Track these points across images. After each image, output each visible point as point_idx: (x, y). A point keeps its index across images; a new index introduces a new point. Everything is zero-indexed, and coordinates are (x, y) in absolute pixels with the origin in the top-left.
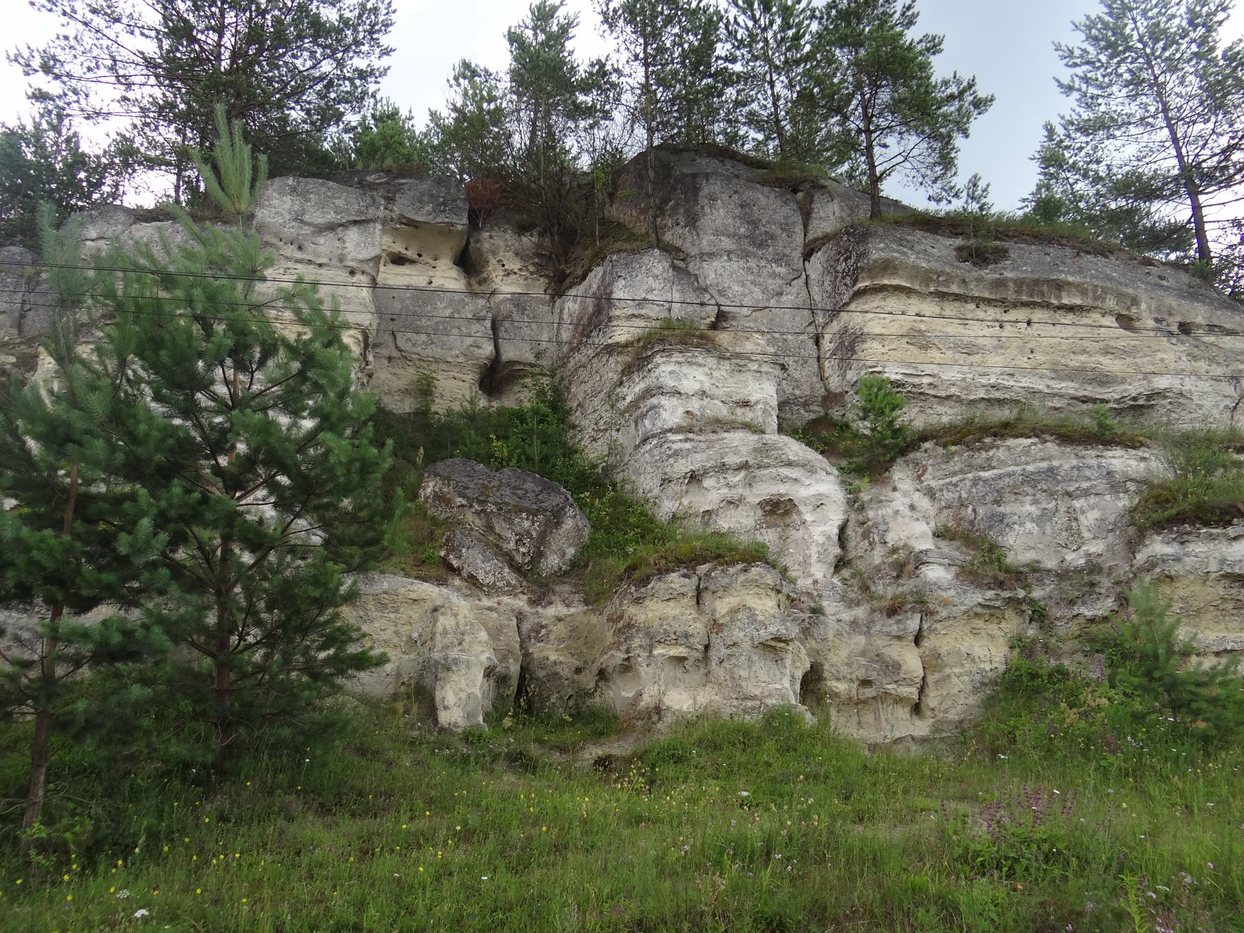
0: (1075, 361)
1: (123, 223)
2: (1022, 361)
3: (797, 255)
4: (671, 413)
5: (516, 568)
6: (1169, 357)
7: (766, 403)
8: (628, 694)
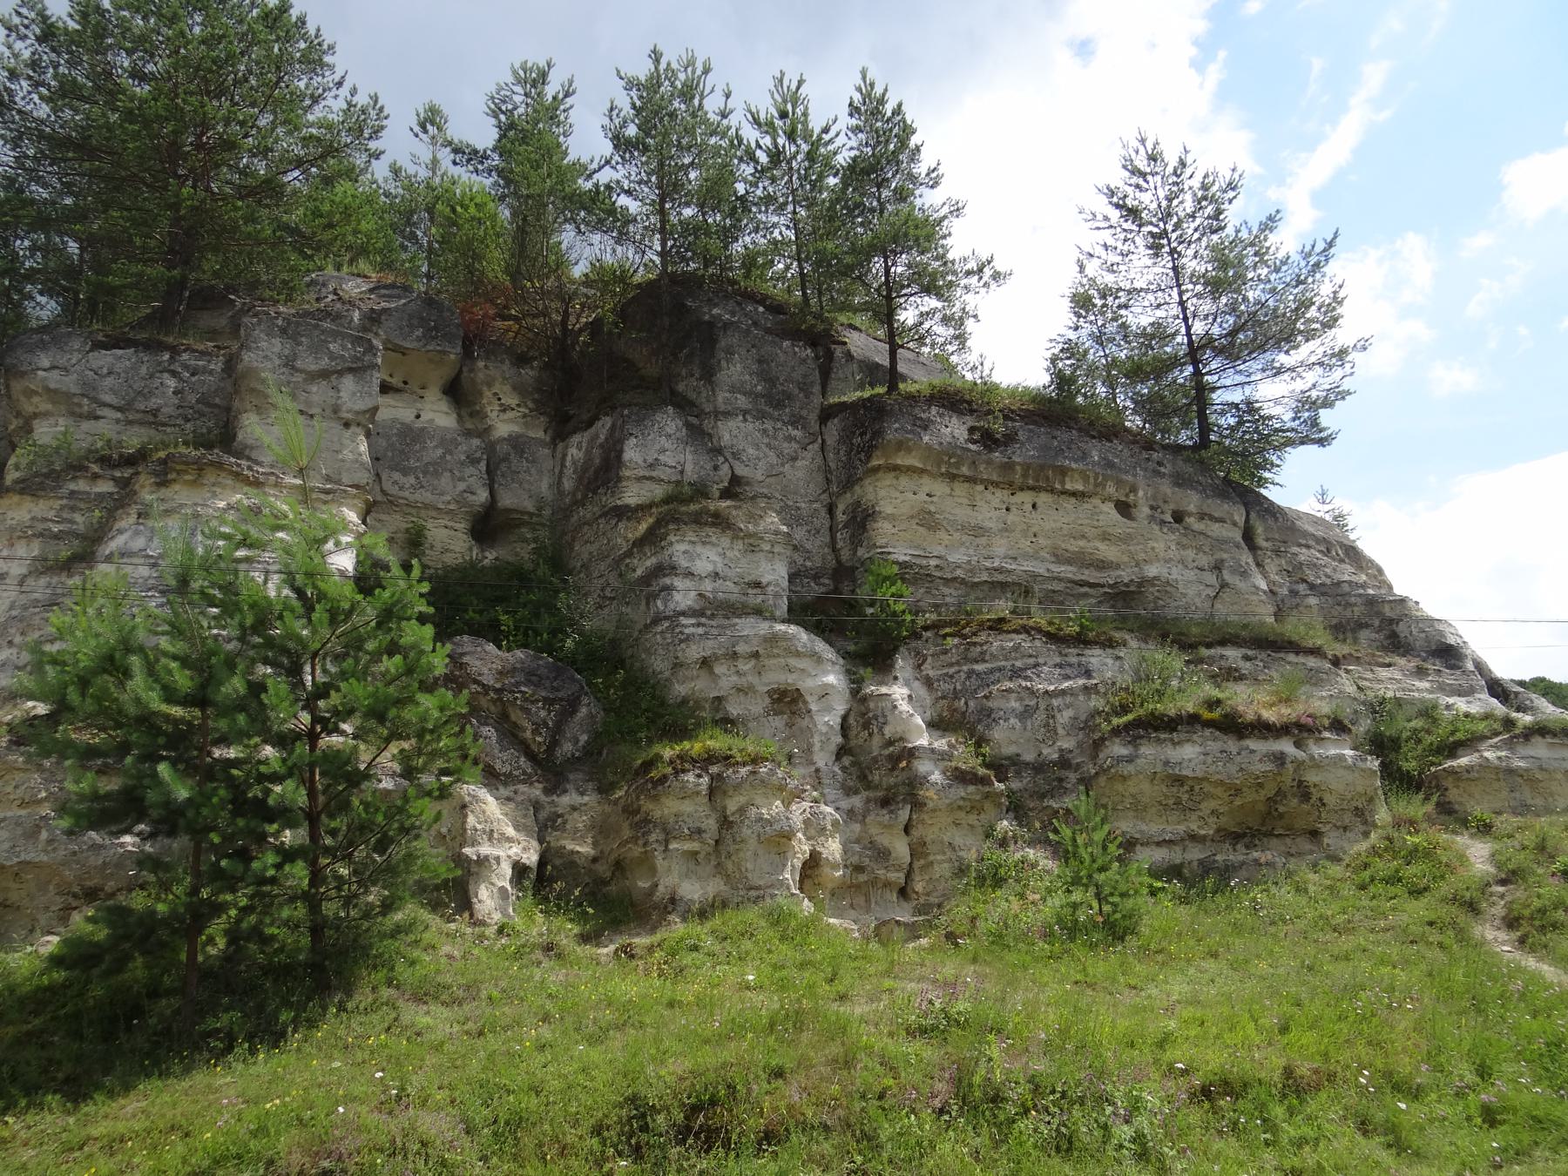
0: (1074, 546)
1: (79, 351)
2: (1025, 544)
3: (813, 418)
4: (683, 596)
5: (531, 756)
6: (1159, 546)
7: (777, 585)
8: (643, 884)
